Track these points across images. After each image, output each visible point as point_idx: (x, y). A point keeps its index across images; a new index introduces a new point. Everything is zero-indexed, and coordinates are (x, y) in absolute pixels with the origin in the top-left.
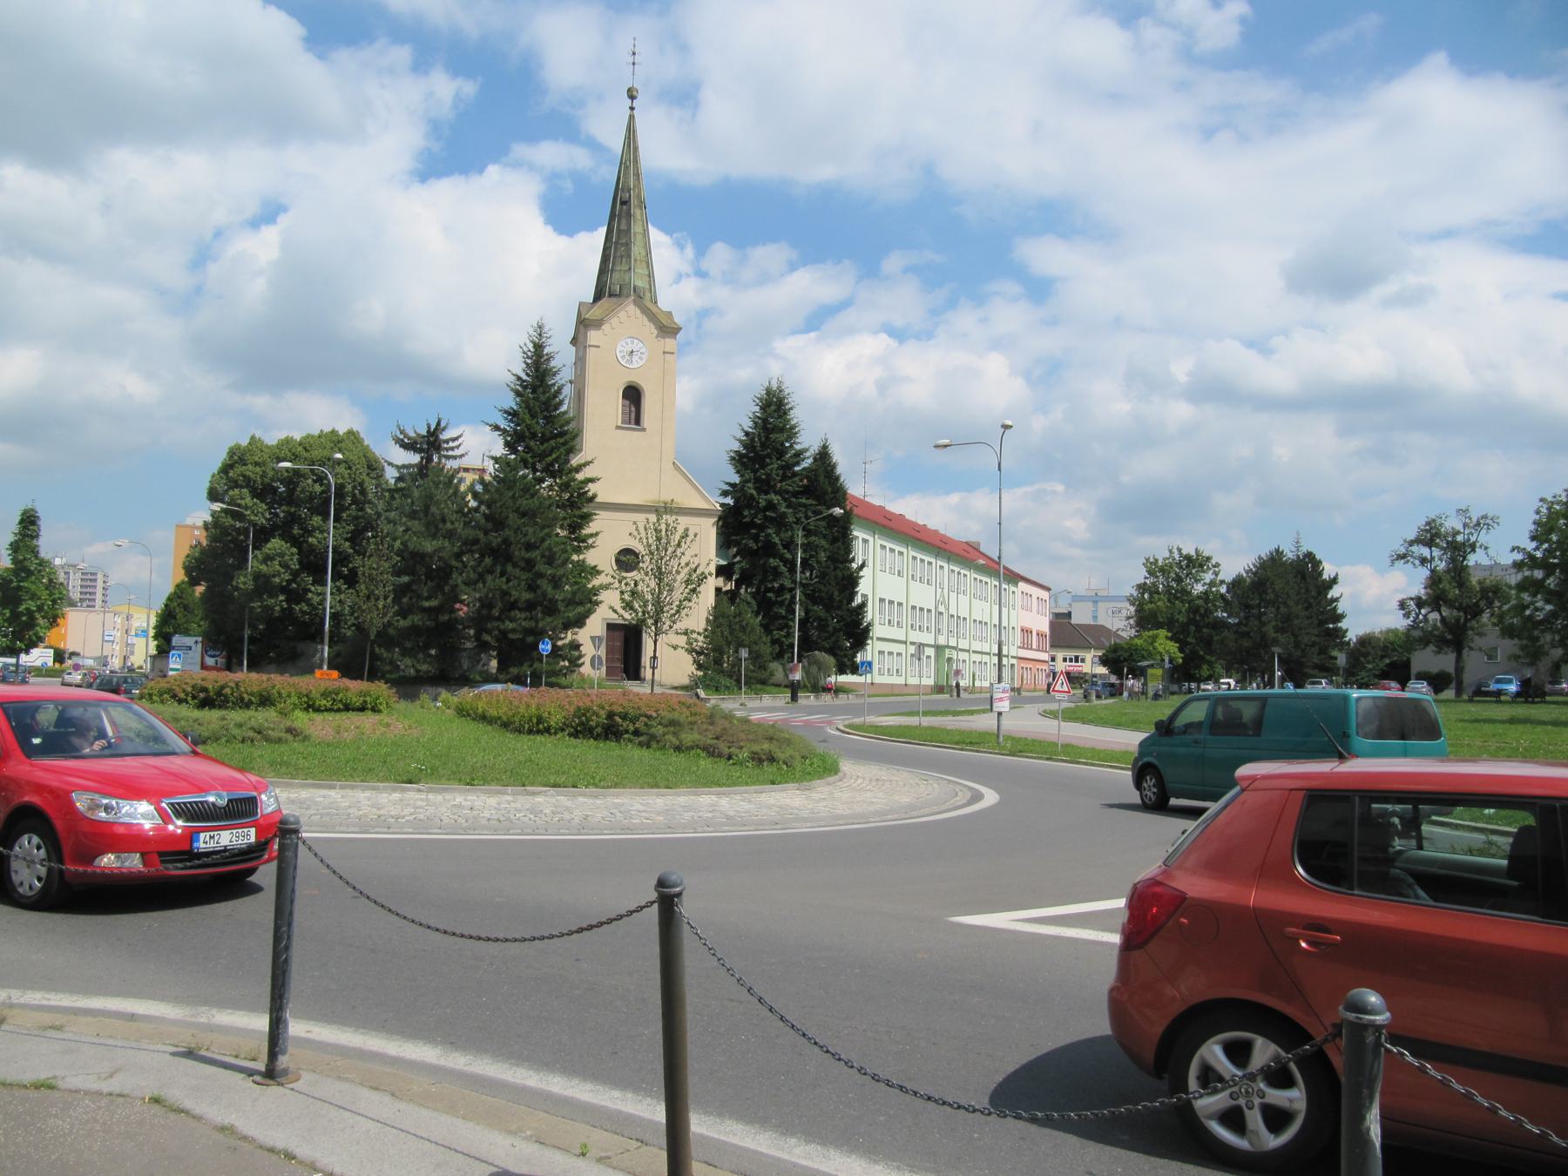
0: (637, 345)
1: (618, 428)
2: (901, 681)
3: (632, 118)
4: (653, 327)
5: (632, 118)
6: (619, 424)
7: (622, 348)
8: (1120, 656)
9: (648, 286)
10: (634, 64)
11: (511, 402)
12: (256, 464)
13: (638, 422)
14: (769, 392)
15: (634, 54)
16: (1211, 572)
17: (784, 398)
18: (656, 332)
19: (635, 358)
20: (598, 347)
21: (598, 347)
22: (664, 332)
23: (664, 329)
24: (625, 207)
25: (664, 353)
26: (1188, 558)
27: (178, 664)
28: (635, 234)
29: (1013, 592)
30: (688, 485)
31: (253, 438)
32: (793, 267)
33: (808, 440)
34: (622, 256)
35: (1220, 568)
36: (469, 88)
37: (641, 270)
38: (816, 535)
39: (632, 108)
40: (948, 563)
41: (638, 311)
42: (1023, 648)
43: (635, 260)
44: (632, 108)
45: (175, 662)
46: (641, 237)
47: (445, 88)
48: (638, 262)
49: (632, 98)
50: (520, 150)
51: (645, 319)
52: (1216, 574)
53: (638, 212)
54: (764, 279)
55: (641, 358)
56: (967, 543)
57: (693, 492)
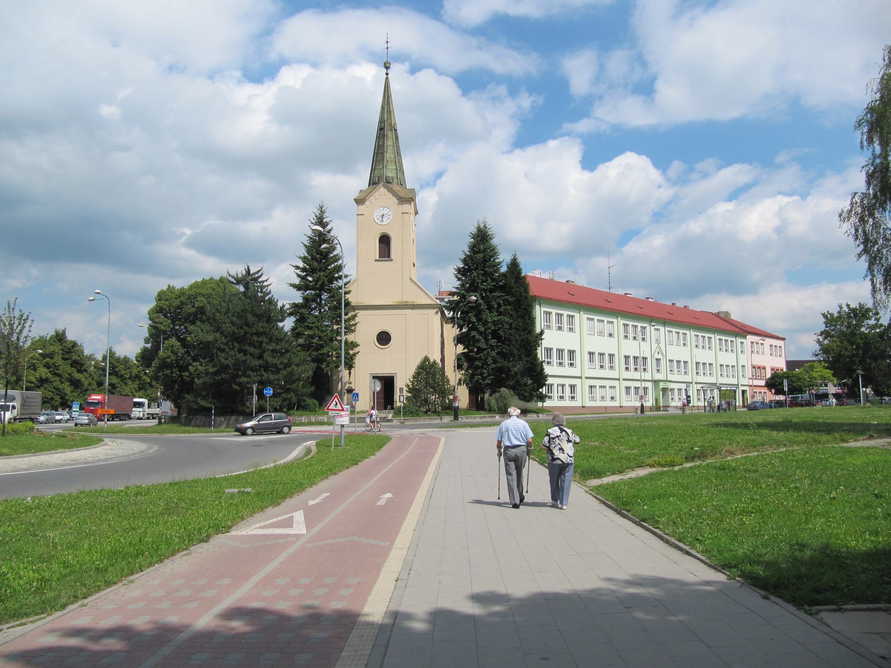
0: (386, 211)
1: (376, 260)
2: (616, 404)
3: (387, 79)
4: (395, 199)
5: (387, 79)
6: (377, 258)
7: (377, 214)
8: (776, 382)
9: (396, 176)
10: (387, 48)
11: (303, 252)
12: (167, 300)
13: (389, 256)
14: (479, 230)
15: (387, 42)
16: (873, 319)
17: (487, 232)
18: (397, 202)
19: (385, 219)
20: (363, 215)
21: (363, 215)
22: (402, 201)
23: (402, 199)
24: (382, 132)
25: (403, 213)
26: (854, 310)
27: (77, 408)
28: (387, 146)
29: (742, 343)
30: (420, 291)
31: (169, 286)
32: (720, 168)
33: (504, 259)
34: (380, 160)
35: (272, 294)
36: (541, 100)
37: (391, 166)
38: (505, 315)
39: (387, 74)
40: (664, 326)
41: (386, 191)
42: (756, 379)
43: (387, 162)
44: (387, 74)
45: (76, 407)
46: (391, 147)
47: (526, 101)
48: (389, 162)
49: (387, 68)
50: (567, 127)
51: (391, 195)
52: (878, 320)
53: (390, 134)
54: (706, 175)
55: (388, 218)
56: (717, 315)
57: (424, 295)
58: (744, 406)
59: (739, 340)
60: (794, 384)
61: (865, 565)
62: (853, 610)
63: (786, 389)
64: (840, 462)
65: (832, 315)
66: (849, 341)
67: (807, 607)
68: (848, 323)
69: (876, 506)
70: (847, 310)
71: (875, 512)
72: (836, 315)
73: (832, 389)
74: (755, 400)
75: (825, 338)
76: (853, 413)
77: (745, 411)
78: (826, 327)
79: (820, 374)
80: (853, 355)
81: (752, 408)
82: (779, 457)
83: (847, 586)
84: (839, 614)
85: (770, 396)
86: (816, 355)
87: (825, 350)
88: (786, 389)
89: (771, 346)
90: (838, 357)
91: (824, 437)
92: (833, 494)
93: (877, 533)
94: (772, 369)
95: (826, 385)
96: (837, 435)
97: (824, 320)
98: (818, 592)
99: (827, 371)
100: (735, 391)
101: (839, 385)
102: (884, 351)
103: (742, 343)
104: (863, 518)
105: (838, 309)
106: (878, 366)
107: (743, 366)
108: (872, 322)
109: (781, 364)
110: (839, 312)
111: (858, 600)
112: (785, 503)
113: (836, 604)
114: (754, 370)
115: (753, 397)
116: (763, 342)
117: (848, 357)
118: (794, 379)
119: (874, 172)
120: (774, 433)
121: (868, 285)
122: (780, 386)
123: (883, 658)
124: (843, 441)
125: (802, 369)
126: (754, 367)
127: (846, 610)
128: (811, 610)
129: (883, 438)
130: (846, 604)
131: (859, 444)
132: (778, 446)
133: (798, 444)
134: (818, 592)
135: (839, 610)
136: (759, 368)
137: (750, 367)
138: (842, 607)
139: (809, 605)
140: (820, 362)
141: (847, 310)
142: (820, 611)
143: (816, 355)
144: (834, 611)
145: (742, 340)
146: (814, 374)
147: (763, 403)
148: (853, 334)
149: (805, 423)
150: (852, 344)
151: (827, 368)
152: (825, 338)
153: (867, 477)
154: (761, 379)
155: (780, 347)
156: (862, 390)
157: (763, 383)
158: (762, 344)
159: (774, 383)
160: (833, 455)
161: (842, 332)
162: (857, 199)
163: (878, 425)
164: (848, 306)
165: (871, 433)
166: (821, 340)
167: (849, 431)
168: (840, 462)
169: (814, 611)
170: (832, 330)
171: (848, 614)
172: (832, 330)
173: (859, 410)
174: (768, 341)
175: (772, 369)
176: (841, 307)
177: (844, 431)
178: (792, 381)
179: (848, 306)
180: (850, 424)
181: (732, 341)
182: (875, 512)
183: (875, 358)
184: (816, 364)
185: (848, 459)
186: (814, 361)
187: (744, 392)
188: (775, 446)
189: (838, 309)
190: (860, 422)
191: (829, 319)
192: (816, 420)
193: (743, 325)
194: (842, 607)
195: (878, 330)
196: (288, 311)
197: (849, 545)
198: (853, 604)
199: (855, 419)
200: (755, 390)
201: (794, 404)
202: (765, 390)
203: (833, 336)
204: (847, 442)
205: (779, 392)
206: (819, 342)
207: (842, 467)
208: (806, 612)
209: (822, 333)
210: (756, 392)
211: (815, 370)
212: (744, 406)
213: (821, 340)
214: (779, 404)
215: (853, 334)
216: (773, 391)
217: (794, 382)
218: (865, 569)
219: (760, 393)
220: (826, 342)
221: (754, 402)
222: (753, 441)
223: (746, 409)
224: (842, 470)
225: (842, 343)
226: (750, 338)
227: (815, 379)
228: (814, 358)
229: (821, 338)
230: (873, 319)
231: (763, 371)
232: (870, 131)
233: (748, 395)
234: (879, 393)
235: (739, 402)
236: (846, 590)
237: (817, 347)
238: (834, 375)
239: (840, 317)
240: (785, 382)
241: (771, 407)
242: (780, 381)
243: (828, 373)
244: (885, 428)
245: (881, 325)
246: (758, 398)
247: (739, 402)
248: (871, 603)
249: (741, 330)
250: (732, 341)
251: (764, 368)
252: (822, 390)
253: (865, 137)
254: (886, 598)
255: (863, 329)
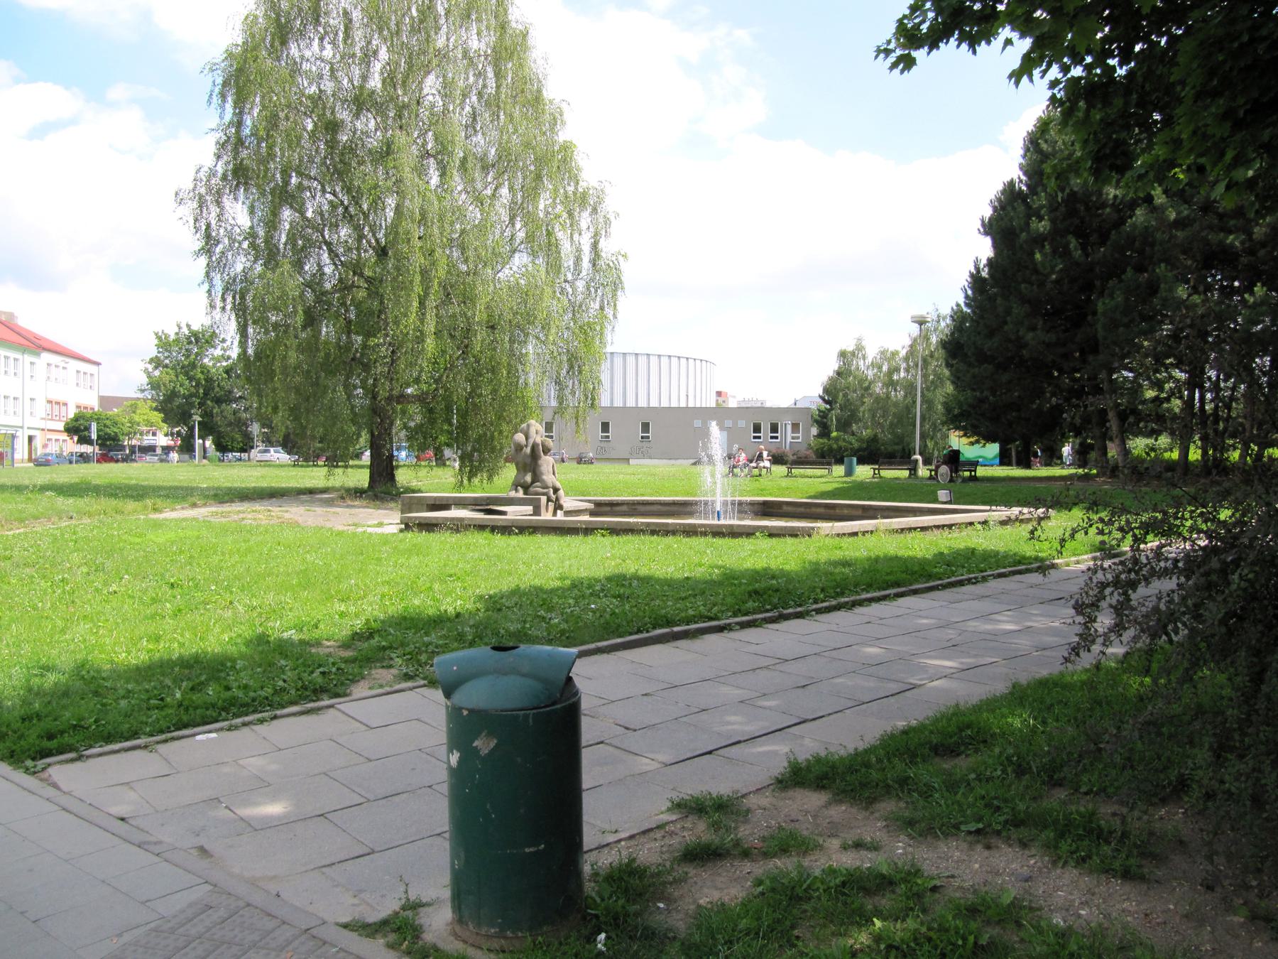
26: (195, 334)
29: (32, 363)
42: (52, 420)
58: (30, 460)
59: (28, 358)
60: (108, 430)
61: (130, 687)
62: (100, 755)
63: (94, 436)
64: (138, 540)
65: (167, 336)
66: (186, 374)
67: (29, 763)
68: (187, 350)
69: (166, 600)
70: (187, 332)
71: (162, 609)
72: (173, 337)
73: (162, 440)
74: (48, 451)
75: (156, 368)
76: (178, 471)
77: (30, 468)
78: (159, 352)
79: (145, 417)
80: (191, 395)
81: (41, 463)
82: (52, 535)
83: (96, 721)
84: (78, 764)
85: (72, 446)
86: (143, 391)
87: (154, 385)
88: (94, 436)
89: (78, 372)
90: (172, 395)
91: (131, 505)
92: (114, 587)
93: (157, 639)
94: (78, 407)
95: (154, 434)
96: (149, 502)
97: (156, 342)
98: (51, 737)
99: (156, 413)
100: (13, 437)
101: (172, 434)
102: (230, 392)
103: (32, 363)
104: (146, 617)
105: (176, 330)
106: (222, 412)
107: (32, 399)
108: (218, 352)
109: (92, 401)
110: (177, 334)
111: (109, 739)
112: (40, 604)
113: (76, 750)
114: (49, 406)
115: (45, 446)
116: (65, 365)
117: (184, 397)
118: (108, 422)
119: (226, 142)
120: (61, 499)
121: (203, 300)
122: (86, 433)
123: (123, 819)
124: (155, 510)
125: (120, 409)
126: (50, 402)
127: (88, 757)
128: (35, 766)
129: (211, 505)
130: (91, 747)
131: (174, 515)
132: (60, 518)
133: (90, 515)
134: (51, 737)
135: (79, 758)
136: (58, 403)
137: (44, 402)
138: (84, 753)
139: (34, 759)
140: (145, 400)
141: (187, 332)
142: (49, 765)
143: (143, 391)
144: (72, 760)
145: (33, 359)
146: (137, 418)
147: (59, 456)
148: (193, 366)
149: (109, 486)
150: (191, 379)
151: (156, 409)
152: (156, 368)
153: (168, 559)
154: (60, 420)
155: (92, 375)
156: (198, 442)
157: (61, 426)
158: (64, 368)
159: (77, 429)
160: (131, 530)
161: (178, 362)
162: (202, 175)
163: (208, 489)
164: (188, 326)
165: (194, 499)
166: (150, 370)
167: (167, 496)
168: (138, 540)
169: (39, 768)
170: (166, 358)
171: (91, 762)
172: (166, 358)
173: (192, 469)
174: (74, 365)
175: (78, 407)
176: (180, 328)
177: (160, 496)
178: (105, 426)
179: (188, 326)
180: (170, 488)
181: (16, 360)
182: (162, 609)
183: (218, 401)
184: (140, 404)
185: (151, 536)
186: (138, 399)
187: (31, 439)
188: (55, 519)
189: (176, 330)
190: (185, 485)
191: (164, 343)
192: (126, 482)
193: (37, 338)
194: (84, 753)
195: (225, 364)
196: (389, 408)
197: (116, 659)
198: (101, 746)
199: (180, 481)
200: (48, 437)
201: (104, 458)
202: (65, 436)
203: (166, 366)
204: (161, 512)
205: (85, 440)
206: (146, 371)
207: (137, 547)
208: (27, 770)
209: (151, 361)
210: (49, 440)
211: (138, 411)
212: (30, 460)
213: (150, 370)
214: (84, 458)
215: (193, 366)
216: (76, 438)
217: (107, 427)
218: (129, 692)
219: (57, 440)
220: (157, 373)
221: (46, 455)
222: (20, 512)
223: (32, 464)
224: (137, 551)
225: (177, 376)
226: (46, 357)
227: (138, 424)
228: (140, 395)
229: (150, 367)
230: (219, 347)
231: (63, 408)
232: (225, 84)
233: (38, 443)
234: (222, 448)
235: (21, 451)
236: (94, 727)
237: (146, 380)
238: (164, 421)
239: (177, 341)
240: (94, 427)
241: (71, 462)
242: (87, 424)
243: (157, 417)
244: (212, 493)
245: (229, 358)
246: (53, 449)
247: (21, 451)
248: (127, 740)
249: (35, 345)
250: (16, 360)
251: (66, 404)
252: (148, 440)
253: (217, 90)
254: (148, 729)
255: (206, 360)
